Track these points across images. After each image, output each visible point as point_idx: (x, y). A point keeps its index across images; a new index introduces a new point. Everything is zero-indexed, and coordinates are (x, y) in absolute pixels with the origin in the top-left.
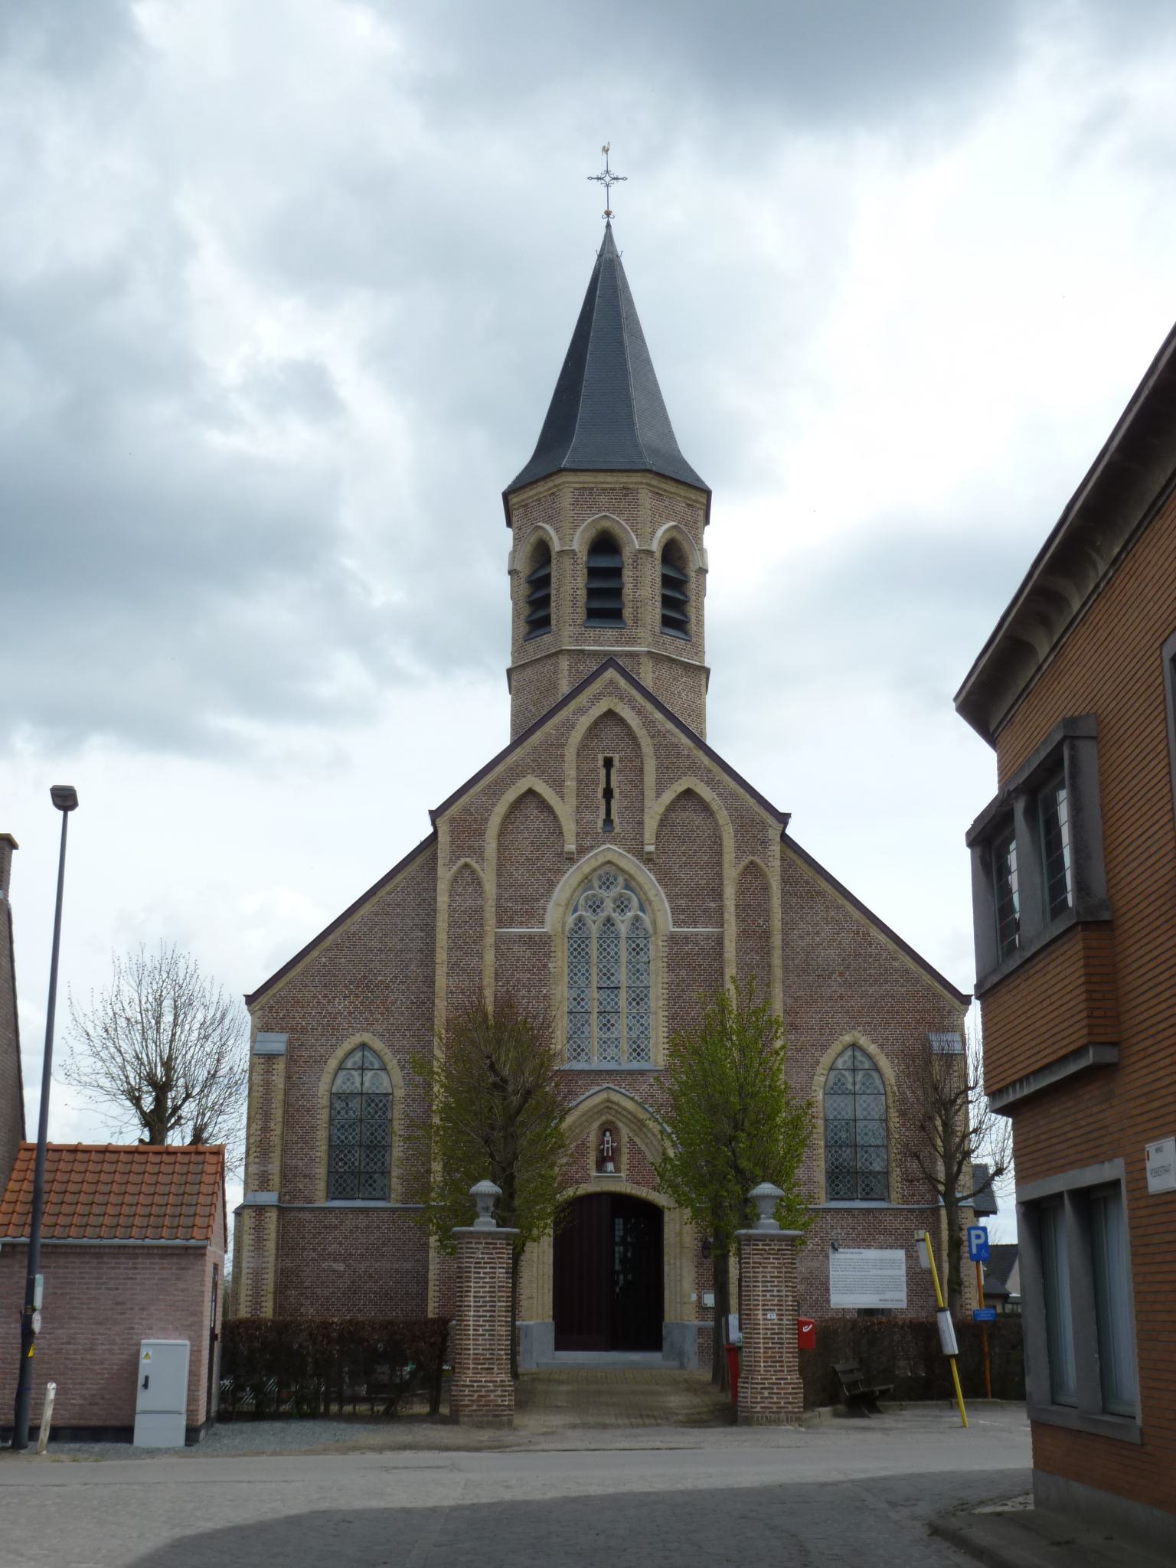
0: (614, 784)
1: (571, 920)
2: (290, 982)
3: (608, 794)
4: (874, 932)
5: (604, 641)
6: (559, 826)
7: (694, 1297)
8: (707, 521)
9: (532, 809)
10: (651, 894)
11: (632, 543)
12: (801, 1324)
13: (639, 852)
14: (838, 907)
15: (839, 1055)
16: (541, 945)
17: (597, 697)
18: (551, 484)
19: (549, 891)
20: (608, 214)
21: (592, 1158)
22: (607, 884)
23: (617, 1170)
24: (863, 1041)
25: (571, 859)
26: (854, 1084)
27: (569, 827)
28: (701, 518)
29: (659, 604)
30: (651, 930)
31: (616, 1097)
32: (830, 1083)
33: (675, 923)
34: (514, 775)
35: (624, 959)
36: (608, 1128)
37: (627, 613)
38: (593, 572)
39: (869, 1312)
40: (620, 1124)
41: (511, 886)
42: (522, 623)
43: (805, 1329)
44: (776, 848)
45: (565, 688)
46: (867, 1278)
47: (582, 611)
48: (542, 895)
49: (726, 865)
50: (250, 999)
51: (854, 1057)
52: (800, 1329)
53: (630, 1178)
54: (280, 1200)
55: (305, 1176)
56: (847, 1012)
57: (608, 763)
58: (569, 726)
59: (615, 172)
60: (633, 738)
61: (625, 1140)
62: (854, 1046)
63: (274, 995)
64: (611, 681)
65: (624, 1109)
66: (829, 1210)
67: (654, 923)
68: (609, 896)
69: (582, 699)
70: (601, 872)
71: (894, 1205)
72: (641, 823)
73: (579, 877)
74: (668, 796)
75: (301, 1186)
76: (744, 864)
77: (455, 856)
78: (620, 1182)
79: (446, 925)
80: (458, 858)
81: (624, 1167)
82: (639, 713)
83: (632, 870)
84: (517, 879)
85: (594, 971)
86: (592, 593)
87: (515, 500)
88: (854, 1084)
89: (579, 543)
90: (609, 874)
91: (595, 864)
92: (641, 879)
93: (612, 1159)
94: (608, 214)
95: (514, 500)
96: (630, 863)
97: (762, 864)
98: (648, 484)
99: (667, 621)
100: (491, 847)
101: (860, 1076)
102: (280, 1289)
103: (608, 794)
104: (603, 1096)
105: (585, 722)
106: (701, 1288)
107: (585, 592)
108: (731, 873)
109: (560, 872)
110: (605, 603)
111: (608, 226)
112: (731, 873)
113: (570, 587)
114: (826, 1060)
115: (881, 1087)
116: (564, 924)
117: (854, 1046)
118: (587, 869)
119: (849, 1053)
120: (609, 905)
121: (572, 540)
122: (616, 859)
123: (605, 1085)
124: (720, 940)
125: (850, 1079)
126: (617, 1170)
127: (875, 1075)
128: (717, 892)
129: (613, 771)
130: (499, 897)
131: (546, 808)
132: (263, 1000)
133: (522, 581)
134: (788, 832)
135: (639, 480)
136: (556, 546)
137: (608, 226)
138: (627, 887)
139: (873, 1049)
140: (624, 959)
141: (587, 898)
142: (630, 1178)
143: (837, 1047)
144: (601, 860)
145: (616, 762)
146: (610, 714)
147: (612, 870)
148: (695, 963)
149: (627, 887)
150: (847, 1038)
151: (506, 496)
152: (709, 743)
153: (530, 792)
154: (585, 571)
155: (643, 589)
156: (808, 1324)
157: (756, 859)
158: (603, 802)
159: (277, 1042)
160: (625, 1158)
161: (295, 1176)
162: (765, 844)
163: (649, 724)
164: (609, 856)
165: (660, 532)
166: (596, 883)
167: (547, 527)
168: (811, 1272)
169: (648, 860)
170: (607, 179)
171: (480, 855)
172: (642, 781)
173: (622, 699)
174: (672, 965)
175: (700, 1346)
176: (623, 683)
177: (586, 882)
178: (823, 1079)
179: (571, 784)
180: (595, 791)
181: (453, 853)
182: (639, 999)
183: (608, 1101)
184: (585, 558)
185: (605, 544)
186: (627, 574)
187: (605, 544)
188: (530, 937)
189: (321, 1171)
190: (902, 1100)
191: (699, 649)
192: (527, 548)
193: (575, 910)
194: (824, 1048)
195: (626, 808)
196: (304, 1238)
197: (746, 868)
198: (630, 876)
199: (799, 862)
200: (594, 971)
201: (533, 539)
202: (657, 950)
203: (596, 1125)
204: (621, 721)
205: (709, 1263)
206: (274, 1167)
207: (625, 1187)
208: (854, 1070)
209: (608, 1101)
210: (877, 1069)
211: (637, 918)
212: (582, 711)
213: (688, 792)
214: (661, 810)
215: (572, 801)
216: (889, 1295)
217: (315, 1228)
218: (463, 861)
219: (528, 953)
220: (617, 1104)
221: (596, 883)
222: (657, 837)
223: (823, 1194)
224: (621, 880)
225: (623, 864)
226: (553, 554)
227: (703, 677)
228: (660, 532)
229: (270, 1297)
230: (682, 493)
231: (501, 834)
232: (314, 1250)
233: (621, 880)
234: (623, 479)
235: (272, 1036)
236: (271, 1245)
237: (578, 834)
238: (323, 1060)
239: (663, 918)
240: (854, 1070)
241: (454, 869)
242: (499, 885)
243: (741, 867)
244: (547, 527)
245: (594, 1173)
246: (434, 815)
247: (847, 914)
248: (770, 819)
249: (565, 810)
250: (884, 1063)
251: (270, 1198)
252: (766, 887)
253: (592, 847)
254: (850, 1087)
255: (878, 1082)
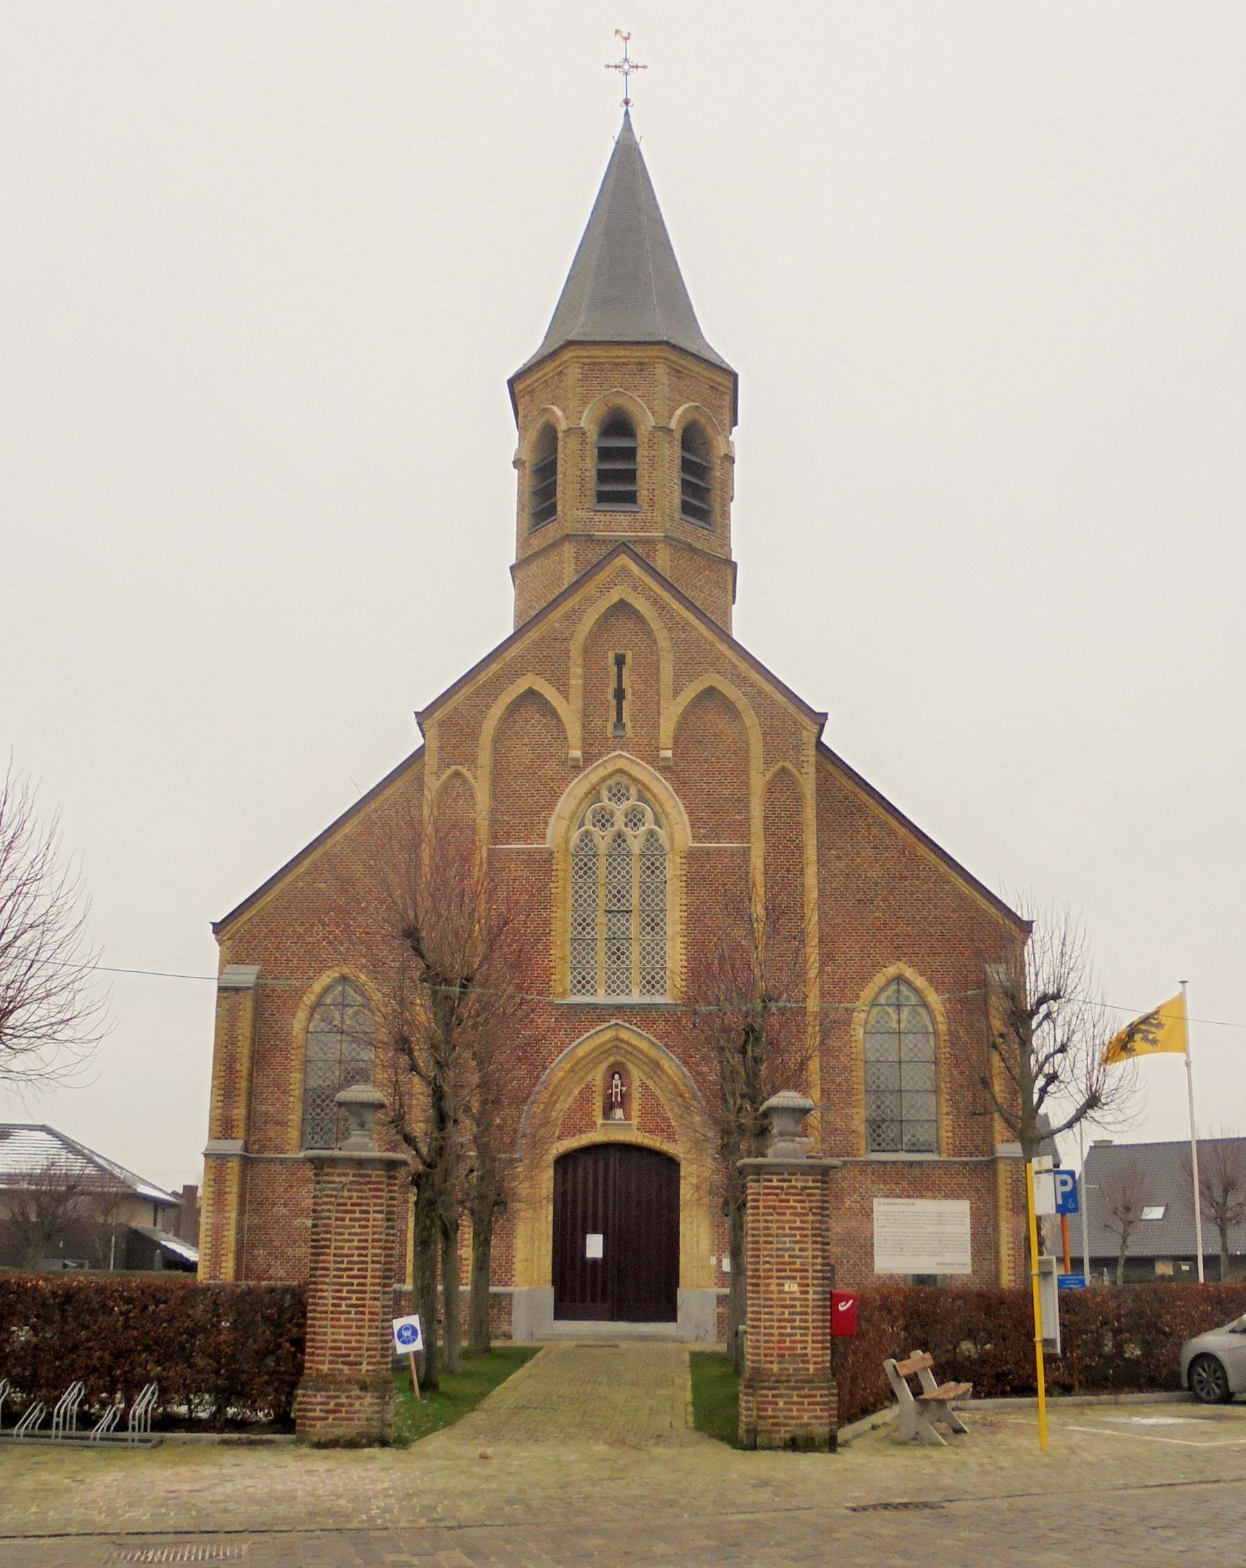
0: (626, 684)
1: (575, 836)
2: (262, 909)
3: (620, 694)
4: (922, 850)
5: (617, 524)
6: (564, 731)
7: (713, 1261)
8: (735, 423)
9: (532, 715)
10: (668, 806)
11: (646, 422)
12: (835, 1299)
13: (654, 760)
14: (882, 824)
15: (883, 989)
16: (545, 862)
17: (605, 589)
18: (557, 363)
19: (551, 805)
20: (627, 102)
21: (598, 1104)
22: (618, 795)
23: (627, 1117)
24: (909, 973)
25: (577, 769)
26: (899, 1021)
27: (574, 730)
28: (727, 418)
29: (678, 488)
30: (667, 846)
31: (625, 1035)
32: (872, 1021)
33: (695, 838)
34: (513, 673)
35: (636, 880)
36: (617, 1070)
37: (643, 495)
38: (605, 454)
39: (922, 1280)
40: (630, 1066)
41: (508, 797)
42: (526, 515)
43: (843, 1307)
44: (811, 751)
45: (569, 577)
46: (921, 1238)
47: (591, 494)
48: (544, 807)
49: (753, 773)
50: (218, 928)
51: (899, 991)
52: (834, 1306)
53: (643, 1127)
54: (246, 1149)
55: (277, 1123)
56: (892, 941)
57: (620, 661)
58: (572, 618)
59: (634, 59)
60: (649, 633)
61: (636, 1084)
62: (899, 979)
63: (245, 923)
64: (623, 567)
65: (635, 1048)
66: (868, 1163)
67: (672, 838)
68: (619, 811)
69: (590, 588)
70: (611, 782)
71: (944, 1157)
72: (656, 727)
73: (586, 786)
74: (690, 693)
75: (272, 1134)
76: (773, 770)
77: (444, 764)
78: (627, 1129)
79: (583, 1136)
80: (448, 766)
81: (635, 1114)
82: (655, 602)
83: (646, 779)
84: (514, 791)
85: (602, 892)
86: (603, 476)
87: (521, 387)
88: (899, 1021)
89: (589, 420)
90: (620, 786)
91: (603, 772)
92: (656, 789)
93: (621, 1105)
94: (627, 102)
95: (520, 387)
96: (644, 772)
97: (794, 771)
98: (665, 358)
99: (687, 509)
100: (485, 756)
101: (905, 1014)
102: (242, 1249)
103: (620, 694)
104: (609, 1035)
105: (592, 615)
106: (718, 1249)
107: (594, 473)
108: (758, 781)
109: (565, 781)
110: (617, 481)
111: (627, 114)
112: (758, 781)
113: (577, 467)
114: (867, 993)
115: (929, 1024)
116: (567, 840)
117: (899, 979)
118: (594, 778)
119: (894, 987)
120: (619, 821)
121: (579, 418)
122: (627, 767)
123: (613, 1022)
124: (746, 852)
125: (895, 1017)
126: (627, 1117)
127: (923, 1011)
128: (743, 804)
129: (625, 670)
130: (494, 811)
131: (548, 710)
132: (233, 928)
133: (527, 471)
134: (823, 739)
135: (656, 354)
136: (562, 426)
137: (627, 114)
138: (641, 798)
139: (920, 982)
140: (636, 880)
141: (595, 811)
142: (643, 1127)
143: (879, 980)
144: (611, 768)
145: (629, 660)
146: (622, 605)
147: (625, 781)
148: (715, 884)
149: (641, 798)
150: (892, 971)
151: (511, 383)
152: (736, 636)
153: (531, 693)
154: (596, 451)
155: (659, 475)
156: (846, 1298)
157: (788, 765)
158: (614, 702)
159: (247, 975)
160: (635, 1105)
161: (266, 1123)
162: (799, 748)
163: (662, 608)
164: (621, 764)
165: (679, 412)
166: (605, 794)
167: (555, 408)
168: (849, 1233)
169: (665, 769)
170: (626, 67)
171: (472, 761)
172: (658, 681)
173: (635, 589)
174: (693, 882)
175: (720, 1316)
176: (636, 570)
177: (593, 794)
178: (863, 1015)
179: (576, 682)
180: (603, 692)
181: (442, 760)
182: (654, 924)
183: (617, 1039)
184: (595, 437)
185: (618, 424)
186: (642, 453)
187: (618, 424)
188: (529, 853)
189: (295, 1118)
190: (954, 1040)
191: (725, 541)
192: (533, 435)
193: (582, 824)
194: (864, 979)
195: (640, 711)
196: (274, 1191)
197: (776, 775)
198: (644, 786)
199: (836, 773)
200: (602, 892)
201: (540, 423)
202: (673, 869)
203: (603, 1067)
204: (636, 614)
205: (728, 1222)
206: (239, 1112)
207: (635, 1136)
208: (898, 1007)
209: (617, 1039)
210: (925, 1005)
211: (652, 833)
212: (590, 601)
213: (710, 692)
214: (680, 710)
215: (577, 703)
216: (949, 1258)
217: (286, 1181)
218: (453, 768)
219: (526, 873)
220: (628, 1043)
221: (605, 794)
222: (675, 743)
223: (862, 1143)
224: (633, 791)
225: (635, 771)
226: (560, 435)
227: (729, 571)
228: (679, 412)
229: (231, 1256)
230: (706, 374)
231: (497, 740)
232: (285, 1205)
233: (633, 791)
234: (638, 353)
235: (243, 968)
236: (232, 1199)
237: (584, 739)
238: (299, 993)
239: (680, 832)
240: (898, 1007)
241: (444, 777)
242: (494, 797)
243: (769, 775)
244: (555, 408)
245: (600, 1121)
246: (422, 717)
247: (892, 833)
248: (805, 720)
249: (569, 712)
250: (933, 998)
251: (235, 1146)
252: (799, 798)
253: (600, 755)
254: (895, 1025)
255: (927, 1019)
